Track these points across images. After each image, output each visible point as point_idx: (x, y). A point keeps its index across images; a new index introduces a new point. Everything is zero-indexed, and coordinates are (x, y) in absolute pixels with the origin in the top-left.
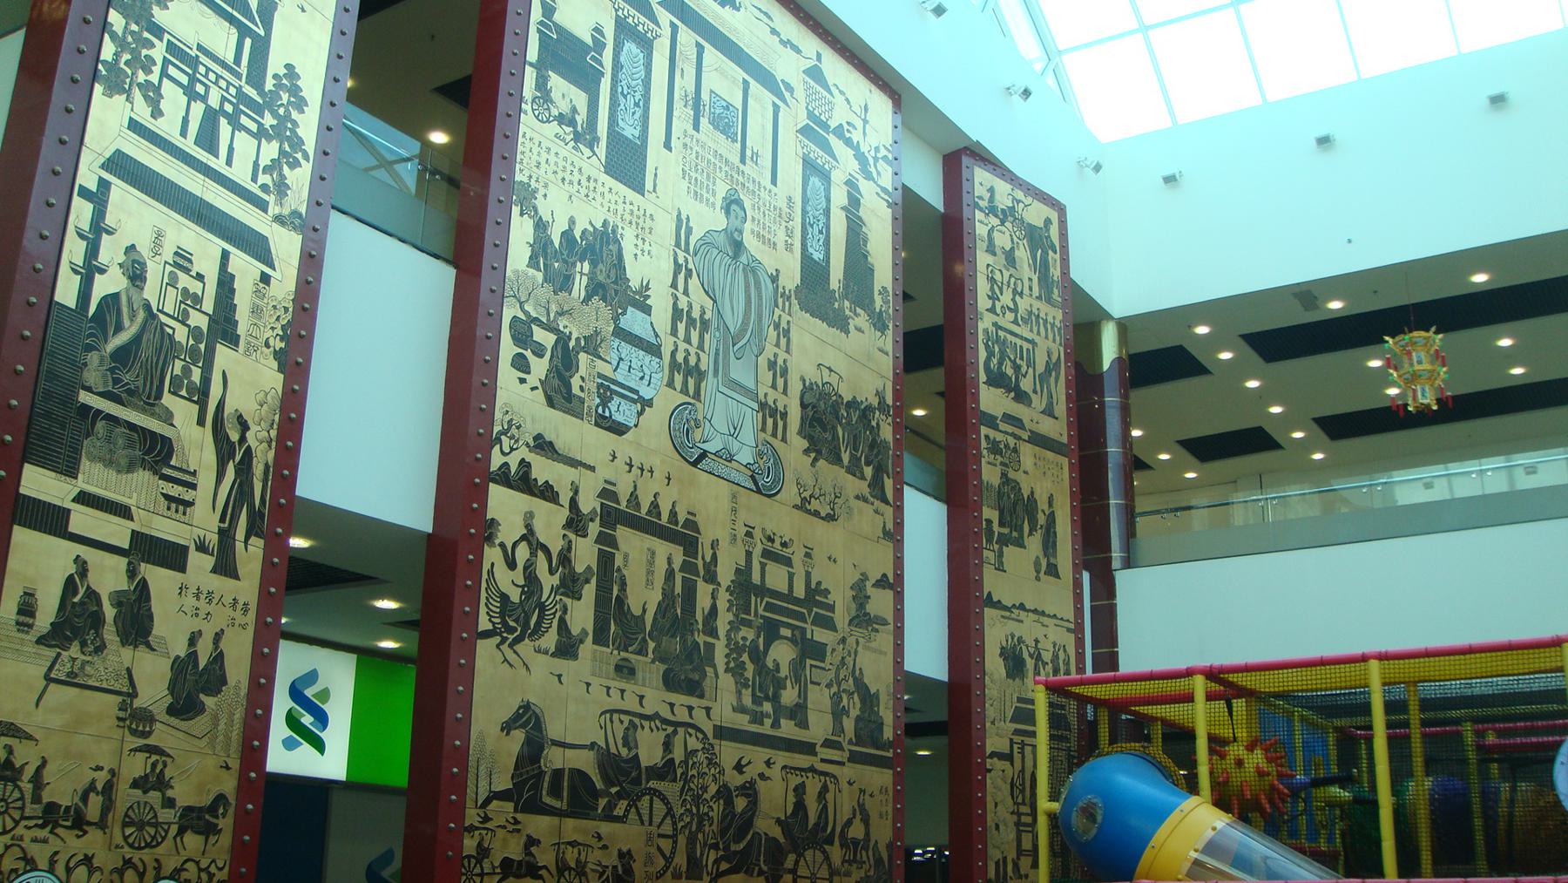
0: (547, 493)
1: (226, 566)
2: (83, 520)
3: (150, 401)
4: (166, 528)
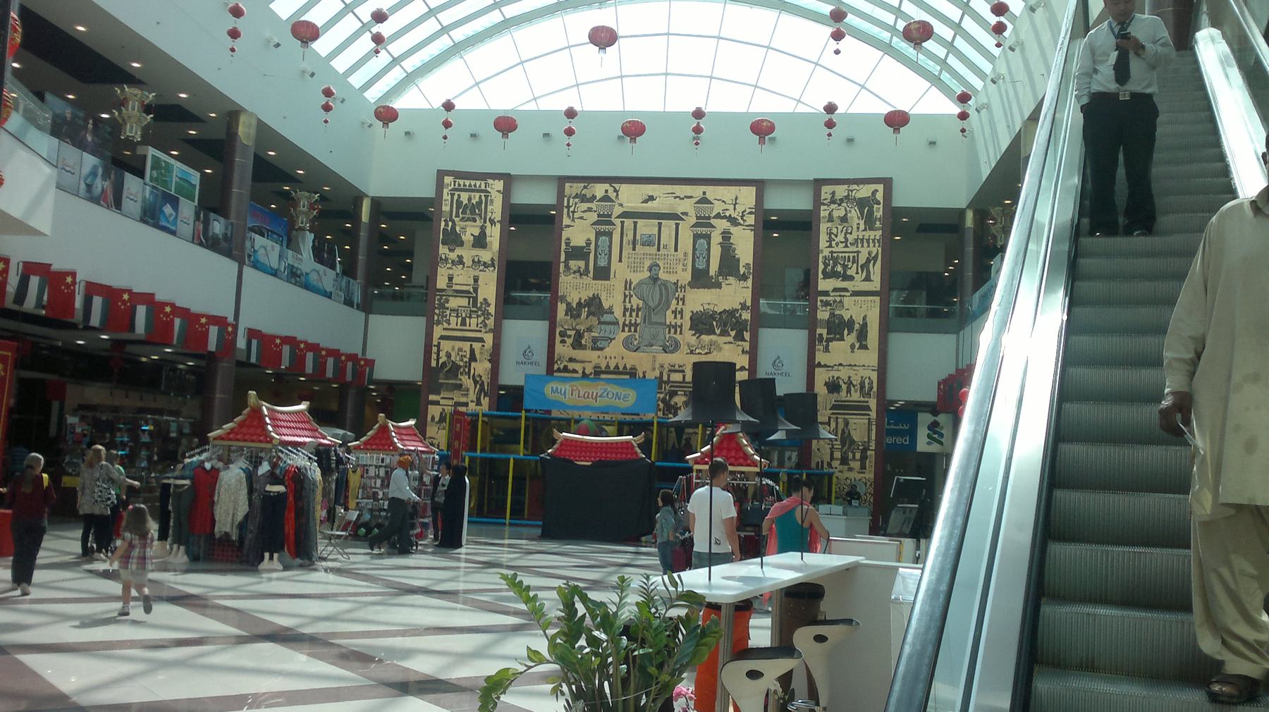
0: (575, 371)
1: (479, 403)
4: (463, 400)
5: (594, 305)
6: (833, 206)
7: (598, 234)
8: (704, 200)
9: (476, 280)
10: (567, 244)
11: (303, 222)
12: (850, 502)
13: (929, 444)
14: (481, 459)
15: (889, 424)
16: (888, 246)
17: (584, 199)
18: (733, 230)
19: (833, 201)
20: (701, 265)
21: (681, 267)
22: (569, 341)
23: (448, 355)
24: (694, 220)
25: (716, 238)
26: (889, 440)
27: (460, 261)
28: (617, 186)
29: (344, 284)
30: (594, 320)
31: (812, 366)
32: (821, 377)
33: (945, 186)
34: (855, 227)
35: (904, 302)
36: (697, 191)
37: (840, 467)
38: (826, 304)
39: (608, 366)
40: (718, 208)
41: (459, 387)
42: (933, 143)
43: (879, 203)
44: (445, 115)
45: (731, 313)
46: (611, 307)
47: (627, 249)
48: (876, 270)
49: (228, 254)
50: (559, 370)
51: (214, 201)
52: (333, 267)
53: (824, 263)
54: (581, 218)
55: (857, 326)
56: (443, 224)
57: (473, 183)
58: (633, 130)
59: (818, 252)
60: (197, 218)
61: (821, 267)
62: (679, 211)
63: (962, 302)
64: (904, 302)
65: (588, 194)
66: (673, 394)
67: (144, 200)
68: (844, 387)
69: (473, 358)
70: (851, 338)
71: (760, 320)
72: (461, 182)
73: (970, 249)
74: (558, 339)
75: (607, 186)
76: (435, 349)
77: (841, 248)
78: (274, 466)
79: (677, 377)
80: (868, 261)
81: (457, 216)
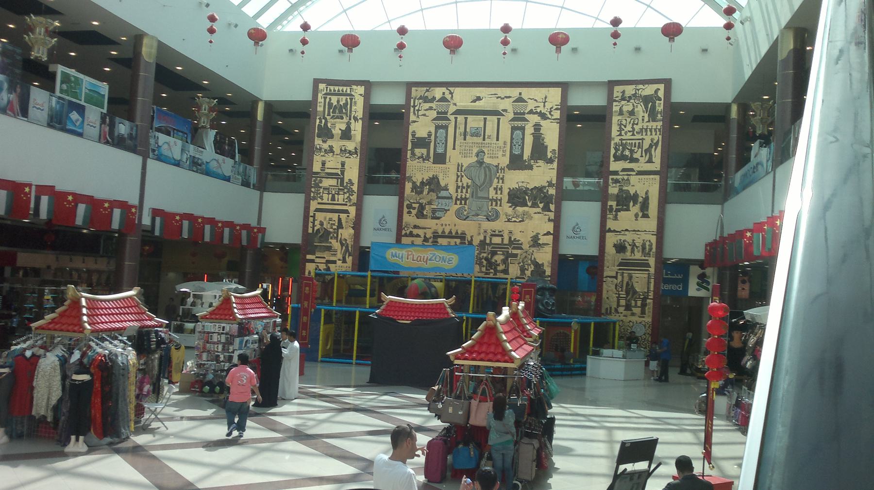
0: (418, 236)
2: (317, 260)
3: (327, 241)
5: (433, 184)
6: (623, 102)
7: (437, 128)
8: (520, 100)
9: (343, 164)
10: (413, 136)
11: (204, 121)
12: (629, 345)
13: (698, 290)
14: (337, 312)
15: (667, 274)
16: (668, 133)
17: (426, 100)
18: (543, 123)
19: (623, 99)
20: (517, 152)
21: (501, 153)
22: (414, 212)
23: (322, 224)
24: (511, 116)
25: (529, 130)
26: (667, 287)
27: (331, 150)
28: (452, 89)
29: (241, 170)
30: (433, 196)
31: (604, 231)
32: (611, 240)
33: (714, 84)
34: (640, 119)
35: (681, 179)
36: (515, 92)
37: (625, 313)
38: (616, 181)
39: (443, 232)
40: (531, 105)
41: (329, 248)
42: (705, 50)
43: (660, 99)
44: (303, 35)
45: (540, 189)
46: (446, 185)
47: (460, 139)
48: (657, 154)
49: (133, 150)
50: (406, 235)
51: (121, 104)
52: (233, 157)
53: (615, 148)
54: (424, 115)
55: (640, 199)
56: (318, 121)
57: (341, 88)
58: (453, 43)
59: (610, 139)
60: (103, 121)
61: (613, 151)
62: (500, 108)
63: (727, 180)
64: (681, 179)
65: (429, 95)
66: (494, 253)
67: (51, 109)
68: (629, 248)
69: (340, 226)
70: (635, 209)
71: (563, 195)
72: (332, 88)
73: (734, 135)
74: (405, 210)
75: (444, 89)
76: (311, 219)
77: (629, 136)
78: (84, 355)
79: (497, 240)
80: (651, 146)
81: (329, 115)
